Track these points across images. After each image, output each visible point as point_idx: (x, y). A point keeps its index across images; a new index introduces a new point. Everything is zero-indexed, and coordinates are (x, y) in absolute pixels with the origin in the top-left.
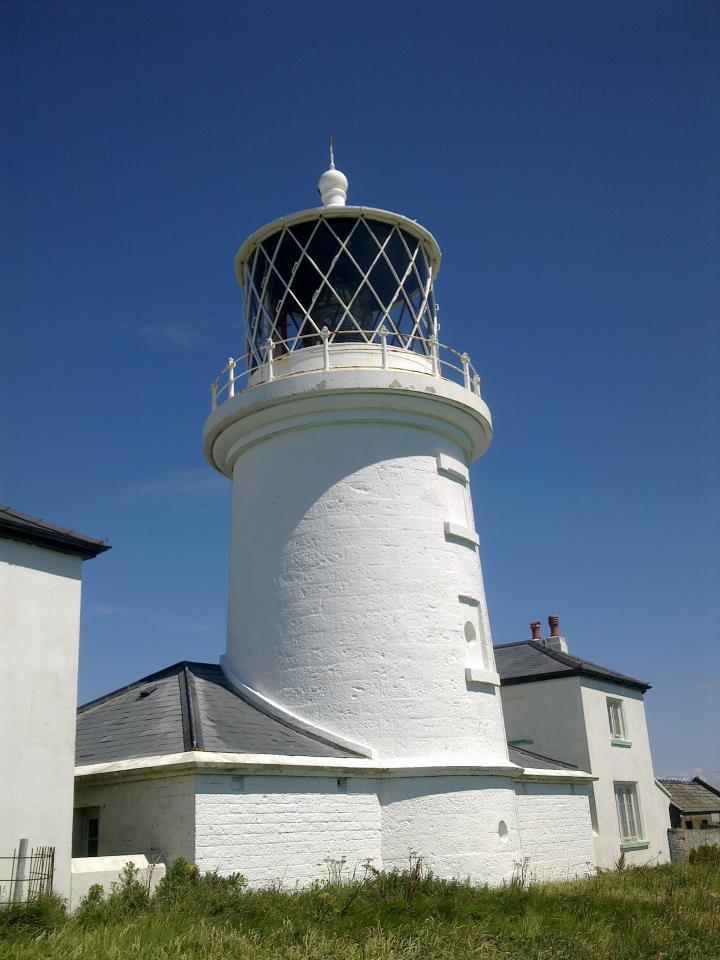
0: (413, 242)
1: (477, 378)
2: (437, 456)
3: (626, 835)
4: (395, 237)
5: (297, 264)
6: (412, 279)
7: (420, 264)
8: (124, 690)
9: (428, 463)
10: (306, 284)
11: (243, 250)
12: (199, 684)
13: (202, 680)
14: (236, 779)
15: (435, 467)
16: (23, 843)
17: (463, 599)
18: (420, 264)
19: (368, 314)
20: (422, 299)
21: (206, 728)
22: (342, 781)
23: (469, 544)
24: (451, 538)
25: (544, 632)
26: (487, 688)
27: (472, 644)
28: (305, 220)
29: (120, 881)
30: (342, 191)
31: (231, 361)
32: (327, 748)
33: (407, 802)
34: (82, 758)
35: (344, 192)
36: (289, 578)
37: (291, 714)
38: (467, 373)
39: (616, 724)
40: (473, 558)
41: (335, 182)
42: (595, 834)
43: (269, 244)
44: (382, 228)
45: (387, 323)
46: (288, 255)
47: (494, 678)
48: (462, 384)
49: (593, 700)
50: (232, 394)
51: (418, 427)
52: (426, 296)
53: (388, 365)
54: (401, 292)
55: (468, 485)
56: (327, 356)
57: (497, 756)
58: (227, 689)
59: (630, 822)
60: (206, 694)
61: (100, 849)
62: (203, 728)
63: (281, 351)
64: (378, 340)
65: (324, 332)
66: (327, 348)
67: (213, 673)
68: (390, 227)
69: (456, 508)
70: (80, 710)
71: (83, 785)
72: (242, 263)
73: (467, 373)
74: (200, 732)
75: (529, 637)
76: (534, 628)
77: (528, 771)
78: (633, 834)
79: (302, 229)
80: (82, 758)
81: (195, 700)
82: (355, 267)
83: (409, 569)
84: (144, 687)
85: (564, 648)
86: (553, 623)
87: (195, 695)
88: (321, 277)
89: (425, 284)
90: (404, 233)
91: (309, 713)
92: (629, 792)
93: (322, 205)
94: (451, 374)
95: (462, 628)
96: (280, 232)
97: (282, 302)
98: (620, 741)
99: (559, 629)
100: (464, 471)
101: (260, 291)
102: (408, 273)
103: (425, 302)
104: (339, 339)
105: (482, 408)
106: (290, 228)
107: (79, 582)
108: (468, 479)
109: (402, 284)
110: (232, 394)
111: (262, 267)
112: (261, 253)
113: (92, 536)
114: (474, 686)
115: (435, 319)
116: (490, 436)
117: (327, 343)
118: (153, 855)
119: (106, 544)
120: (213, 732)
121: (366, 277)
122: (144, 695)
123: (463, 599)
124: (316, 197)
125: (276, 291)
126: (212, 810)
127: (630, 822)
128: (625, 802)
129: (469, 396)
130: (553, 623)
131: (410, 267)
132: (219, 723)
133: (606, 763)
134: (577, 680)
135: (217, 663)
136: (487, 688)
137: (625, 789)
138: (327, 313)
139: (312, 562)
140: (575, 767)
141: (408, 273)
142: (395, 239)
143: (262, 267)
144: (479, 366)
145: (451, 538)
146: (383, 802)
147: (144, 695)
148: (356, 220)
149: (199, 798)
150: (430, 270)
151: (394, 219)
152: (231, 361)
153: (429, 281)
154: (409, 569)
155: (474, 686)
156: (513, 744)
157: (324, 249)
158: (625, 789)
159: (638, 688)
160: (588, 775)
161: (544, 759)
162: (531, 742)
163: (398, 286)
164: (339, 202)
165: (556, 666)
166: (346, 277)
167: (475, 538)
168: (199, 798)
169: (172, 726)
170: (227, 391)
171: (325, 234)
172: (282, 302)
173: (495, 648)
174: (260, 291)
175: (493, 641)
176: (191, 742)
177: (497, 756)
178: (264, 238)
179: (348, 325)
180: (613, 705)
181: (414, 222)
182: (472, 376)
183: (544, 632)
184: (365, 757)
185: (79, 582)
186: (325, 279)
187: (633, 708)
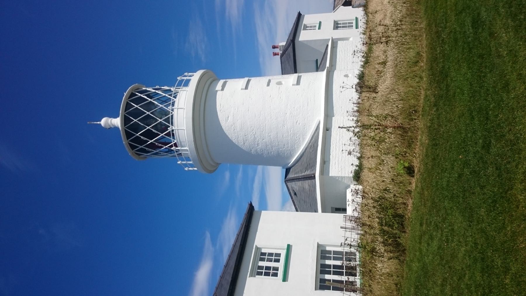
0: (132, 95)
1: (186, 74)
2: (217, 91)
5: (142, 137)
6: (148, 96)
7: (141, 92)
8: (293, 201)
9: (219, 94)
10: (150, 135)
11: (135, 158)
14: (325, 162)
15: (221, 92)
16: (342, 228)
17: (268, 85)
20: (155, 92)
21: (308, 173)
22: (327, 130)
23: (249, 81)
24: (246, 88)
25: (277, 51)
26: (299, 78)
27: (283, 83)
29: (348, 234)
30: (110, 119)
31: (179, 162)
32: (316, 134)
33: (334, 109)
34: (316, 211)
35: (110, 119)
36: (258, 144)
37: (304, 145)
38: (185, 78)
39: (313, 27)
41: (106, 122)
42: (351, 39)
43: (133, 147)
44: (128, 106)
45: (167, 106)
46: (138, 140)
47: (296, 75)
48: (189, 80)
49: (304, 36)
52: (154, 91)
53: (183, 107)
55: (227, 80)
57: (322, 75)
61: (344, 207)
64: (173, 110)
65: (170, 129)
66: (176, 128)
67: (288, 171)
68: (127, 103)
69: (235, 85)
70: (297, 211)
71: (324, 211)
74: (309, 175)
75: (278, 57)
76: (275, 54)
77: (328, 65)
78: (352, 23)
79: (128, 135)
80: (316, 211)
83: (260, 106)
84: (293, 194)
85: (284, 44)
86: (274, 47)
88: (147, 133)
89: (150, 91)
90: (129, 98)
91: (304, 139)
92: (338, 24)
94: (187, 83)
95: (278, 86)
98: (319, 28)
99: (276, 45)
100: (221, 82)
103: (157, 92)
104: (172, 124)
105: (199, 73)
106: (128, 139)
107: (263, 211)
108: (225, 80)
109: (150, 100)
112: (136, 151)
113: (246, 207)
114: (298, 83)
117: (173, 128)
118: (348, 186)
122: (295, 194)
123: (268, 85)
126: (334, 171)
129: (195, 77)
130: (274, 47)
132: (306, 169)
133: (327, 33)
134: (296, 41)
135: (285, 170)
136: (299, 78)
137: (336, 26)
139: (253, 137)
140: (327, 46)
142: (132, 101)
145: (246, 88)
146: (334, 116)
147: (295, 194)
148: (125, 115)
149: (330, 175)
150: (144, 89)
152: (179, 162)
153: (148, 89)
154: (260, 106)
155: (298, 83)
156: (318, 68)
157: (136, 128)
158: (336, 26)
159: (300, 16)
161: (322, 60)
162: (317, 60)
163: (141, 97)
164: (117, 122)
165: (290, 49)
166: (148, 120)
167: (246, 79)
168: (330, 175)
169: (306, 184)
170: (190, 164)
173: (282, 74)
176: (313, 177)
177: (322, 75)
180: (306, 28)
181: (125, 94)
182: (186, 76)
183: (277, 51)
185: (263, 211)
186: (148, 128)
187: (307, 20)
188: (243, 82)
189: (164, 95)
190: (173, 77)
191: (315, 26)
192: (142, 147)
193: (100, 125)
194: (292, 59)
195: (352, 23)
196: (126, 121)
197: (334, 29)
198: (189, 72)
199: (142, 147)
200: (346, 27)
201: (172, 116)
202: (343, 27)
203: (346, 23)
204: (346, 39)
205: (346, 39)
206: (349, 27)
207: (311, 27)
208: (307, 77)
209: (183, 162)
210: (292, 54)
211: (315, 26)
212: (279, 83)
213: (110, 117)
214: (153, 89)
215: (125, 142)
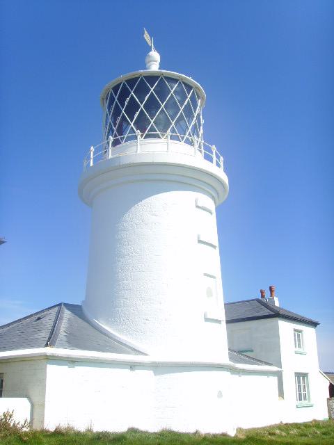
0: (189, 87)
1: (222, 158)
3: (300, 400)
4: (180, 83)
7: (193, 100)
8: (32, 315)
10: (133, 107)
11: (102, 93)
12: (67, 314)
13: (69, 312)
18: (193, 100)
19: (165, 126)
21: (62, 334)
22: (132, 366)
25: (267, 294)
26: (219, 322)
28: (133, 77)
40: (216, 253)
43: (115, 89)
44: (173, 80)
46: (125, 93)
47: (223, 318)
50: (91, 164)
51: (179, 182)
54: (181, 113)
56: (139, 146)
57: (224, 358)
58: (83, 319)
59: (302, 394)
60: (69, 319)
62: (60, 336)
63: (116, 143)
67: (76, 309)
69: (209, 227)
72: (103, 99)
73: (214, 156)
78: (305, 399)
79: (131, 82)
81: (60, 323)
82: (157, 101)
84: (38, 316)
85: (277, 304)
87: (62, 319)
88: (133, 104)
89: (195, 110)
90: (185, 84)
93: (146, 69)
94: (208, 158)
96: (119, 85)
97: (120, 118)
98: (299, 349)
101: (110, 112)
102: (185, 104)
104: (148, 136)
106: (126, 81)
110: (91, 164)
111: (112, 100)
115: (201, 128)
116: (227, 193)
119: (3, 240)
120: (65, 339)
121: (142, 106)
122: (39, 319)
124: (144, 66)
125: (117, 112)
127: (302, 394)
128: (302, 384)
131: (187, 101)
134: (277, 319)
137: (302, 376)
138: (142, 124)
140: (270, 364)
141: (185, 104)
143: (112, 100)
144: (221, 151)
146: (155, 375)
147: (39, 319)
151: (179, 76)
153: (198, 108)
157: (142, 91)
158: (302, 376)
160: (279, 369)
162: (252, 351)
163: (187, 98)
164: (154, 67)
165: (267, 312)
168: (48, 365)
170: (89, 163)
171: (141, 84)
172: (120, 118)
174: (110, 112)
175: (225, 299)
178: (113, 86)
179: (152, 129)
182: (218, 157)
183: (267, 294)
184: (146, 355)
187: (308, 332)
188: (212, 235)
189: (190, 128)
190: (216, 140)
191: (299, 346)
192: (116, 100)
193: (151, 51)
194: (252, 315)
195: (305, 399)
196: (152, 78)
197: (209, 288)
198: (224, 163)
199: (116, 100)
200: (300, 391)
201: (159, 137)
202: (299, 386)
203: (304, 390)
204: (281, 393)
205: (281, 393)
206: (300, 395)
207: (299, 340)
208: (221, 332)
209: (92, 153)
210: (261, 314)
211: (299, 346)
212: (209, 293)
213: (160, 64)
214: (198, 115)
215: (123, 77)
